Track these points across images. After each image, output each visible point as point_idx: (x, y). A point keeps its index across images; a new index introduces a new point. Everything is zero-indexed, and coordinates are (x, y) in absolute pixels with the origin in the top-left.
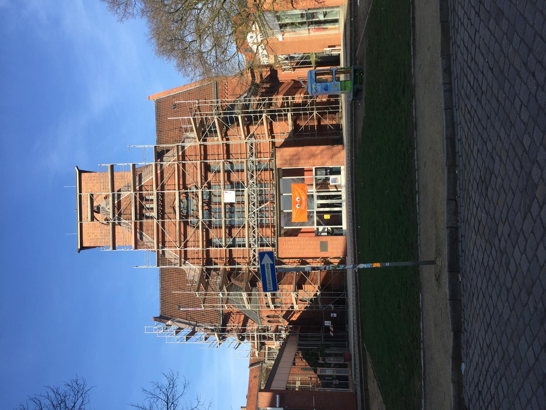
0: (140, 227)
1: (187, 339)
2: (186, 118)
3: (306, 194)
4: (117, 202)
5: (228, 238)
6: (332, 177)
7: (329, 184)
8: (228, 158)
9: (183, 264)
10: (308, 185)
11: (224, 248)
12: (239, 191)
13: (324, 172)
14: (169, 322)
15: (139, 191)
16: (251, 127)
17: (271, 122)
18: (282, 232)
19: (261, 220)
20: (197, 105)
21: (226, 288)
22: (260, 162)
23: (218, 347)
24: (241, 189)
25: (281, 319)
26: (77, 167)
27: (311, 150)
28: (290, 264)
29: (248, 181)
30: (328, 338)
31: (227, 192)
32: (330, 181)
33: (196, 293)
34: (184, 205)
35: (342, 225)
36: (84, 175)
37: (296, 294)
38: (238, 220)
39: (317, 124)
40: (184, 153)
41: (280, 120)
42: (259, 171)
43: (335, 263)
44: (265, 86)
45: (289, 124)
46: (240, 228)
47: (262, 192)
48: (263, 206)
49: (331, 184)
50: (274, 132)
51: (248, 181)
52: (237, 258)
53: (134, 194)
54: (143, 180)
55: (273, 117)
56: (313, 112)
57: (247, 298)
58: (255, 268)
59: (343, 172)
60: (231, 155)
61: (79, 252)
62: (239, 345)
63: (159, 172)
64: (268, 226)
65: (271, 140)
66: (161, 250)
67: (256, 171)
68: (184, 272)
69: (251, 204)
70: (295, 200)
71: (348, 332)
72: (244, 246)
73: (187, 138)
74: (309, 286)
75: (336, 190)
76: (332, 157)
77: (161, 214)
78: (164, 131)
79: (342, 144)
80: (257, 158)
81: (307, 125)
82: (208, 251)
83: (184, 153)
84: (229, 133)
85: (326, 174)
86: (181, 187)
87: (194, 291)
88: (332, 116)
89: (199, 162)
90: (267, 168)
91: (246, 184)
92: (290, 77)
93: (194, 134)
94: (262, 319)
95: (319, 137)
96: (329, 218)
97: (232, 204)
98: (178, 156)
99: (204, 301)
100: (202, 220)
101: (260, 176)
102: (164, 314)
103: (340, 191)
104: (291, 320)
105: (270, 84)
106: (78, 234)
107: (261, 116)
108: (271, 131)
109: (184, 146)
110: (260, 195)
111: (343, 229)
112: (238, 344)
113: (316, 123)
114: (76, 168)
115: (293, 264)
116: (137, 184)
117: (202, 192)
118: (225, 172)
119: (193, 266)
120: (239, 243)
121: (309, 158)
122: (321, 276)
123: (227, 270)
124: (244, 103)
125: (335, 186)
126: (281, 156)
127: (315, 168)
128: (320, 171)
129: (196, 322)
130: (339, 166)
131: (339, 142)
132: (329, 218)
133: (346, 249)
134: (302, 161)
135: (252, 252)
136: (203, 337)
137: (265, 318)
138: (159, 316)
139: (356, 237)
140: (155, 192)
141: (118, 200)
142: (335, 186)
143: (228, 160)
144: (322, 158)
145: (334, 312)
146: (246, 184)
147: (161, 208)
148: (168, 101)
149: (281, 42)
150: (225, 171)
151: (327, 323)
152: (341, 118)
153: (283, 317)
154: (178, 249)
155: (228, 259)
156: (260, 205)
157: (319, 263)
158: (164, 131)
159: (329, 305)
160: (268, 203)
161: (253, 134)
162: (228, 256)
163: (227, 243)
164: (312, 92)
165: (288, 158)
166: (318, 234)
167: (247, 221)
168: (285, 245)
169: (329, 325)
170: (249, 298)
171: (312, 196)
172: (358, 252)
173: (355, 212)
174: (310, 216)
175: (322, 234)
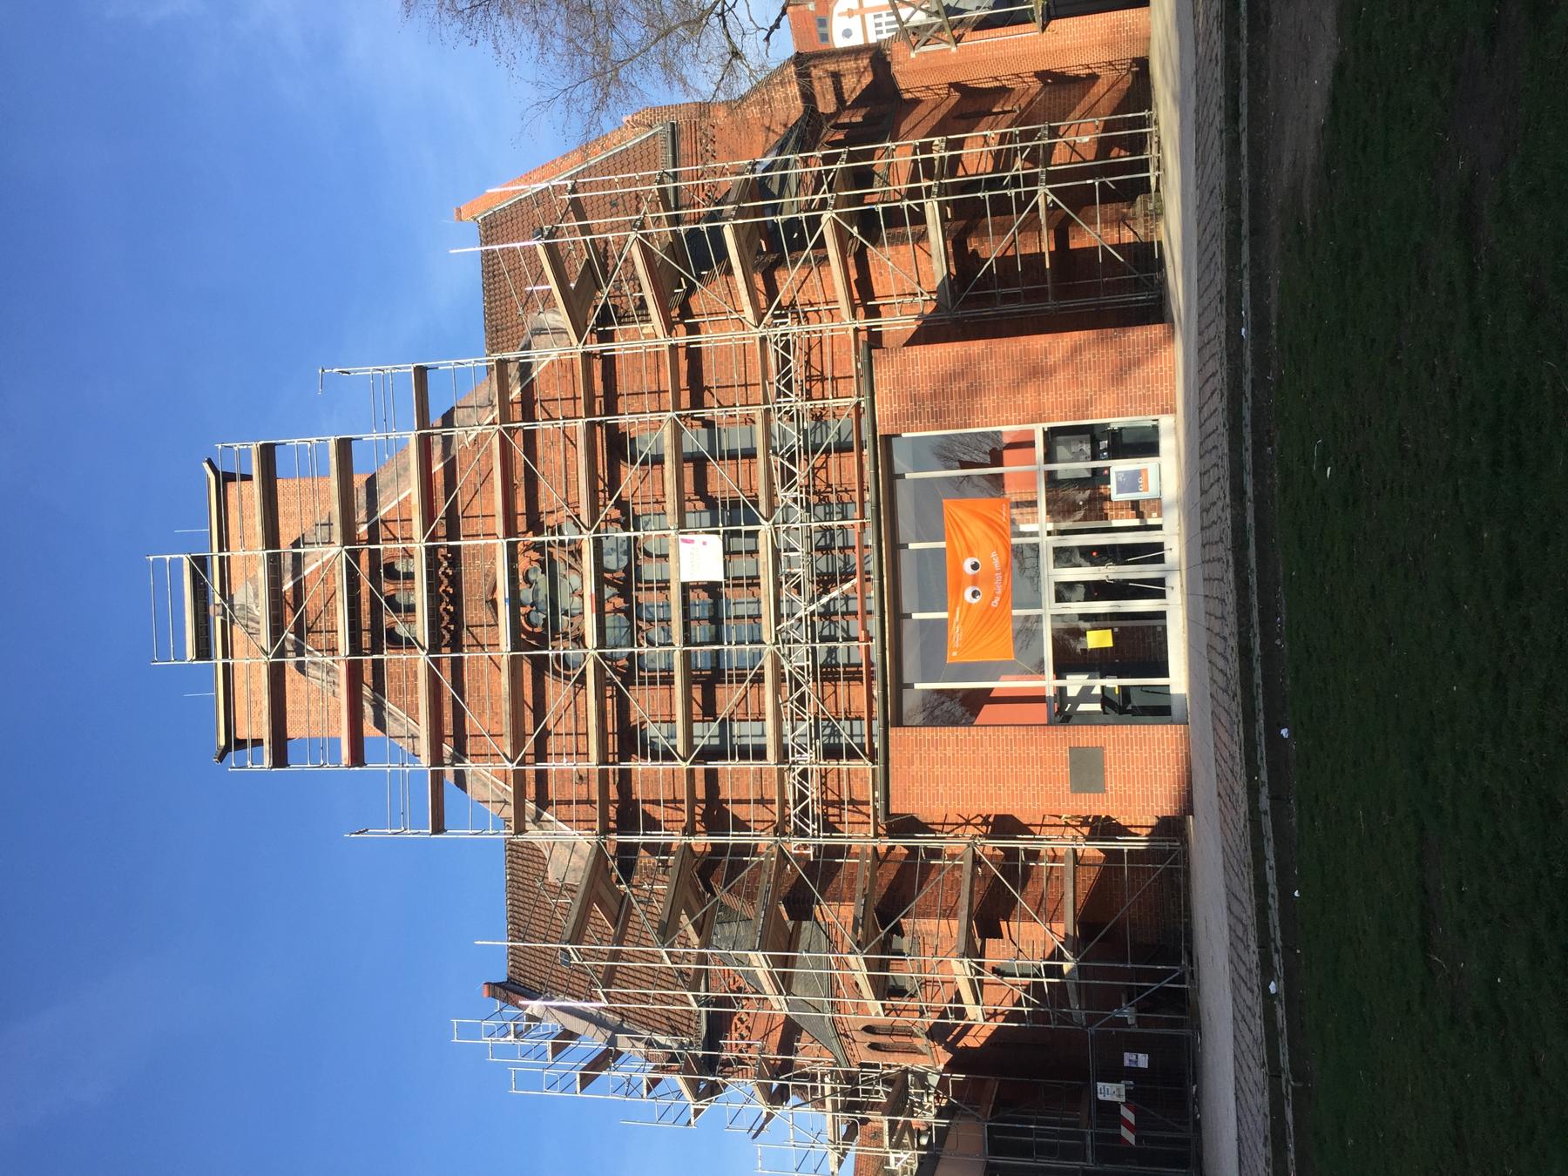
0: (374, 678)
1: (586, 1081)
2: (518, 245)
4: (291, 583)
5: (703, 721)
6: (1119, 467)
7: (1108, 498)
8: (697, 402)
10: (1018, 505)
11: (685, 765)
12: (737, 534)
13: (1087, 448)
14: (535, 1006)
15: (370, 542)
17: (863, 248)
18: (910, 701)
19: (832, 652)
20: (567, 197)
21: (695, 925)
22: (821, 415)
23: (689, 1122)
24: (744, 528)
25: (921, 1042)
26: (210, 462)
27: (1026, 352)
28: (947, 828)
29: (771, 496)
30: (1111, 1149)
32: (1113, 486)
33: (569, 947)
35: (1166, 675)
36: (233, 488)
37: (971, 967)
39: (1053, 248)
40: (528, 392)
41: (897, 240)
43: (1138, 831)
45: (934, 252)
47: (833, 539)
48: (835, 593)
49: (1115, 497)
51: (771, 496)
53: (344, 553)
54: (381, 499)
56: (1036, 191)
58: (805, 847)
59: (1171, 443)
60: (706, 394)
61: (221, 758)
62: (767, 1120)
63: (437, 467)
64: (853, 676)
65: (862, 323)
67: (806, 452)
69: (784, 586)
71: (1198, 1125)
72: (760, 753)
73: (540, 331)
74: (1025, 926)
75: (1136, 522)
76: (1120, 375)
77: (449, 631)
78: (508, 328)
79: (1161, 320)
80: (809, 398)
81: (1010, 253)
82: (625, 776)
83: (528, 392)
85: (1095, 457)
86: (521, 523)
88: (1117, 211)
89: (581, 424)
91: (763, 508)
92: (942, 69)
93: (559, 317)
94: (847, 1036)
95: (1064, 303)
96: (1109, 643)
97: (712, 588)
98: (505, 405)
99: (609, 978)
100: (595, 653)
102: (520, 975)
103: (1159, 527)
104: (960, 1045)
105: (863, 111)
106: (217, 695)
108: (863, 292)
109: (530, 364)
110: (826, 549)
111: (1173, 691)
112: (764, 1115)
113: (1047, 245)
114: (206, 466)
115: (959, 831)
116: (361, 515)
118: (686, 461)
121: (1017, 386)
122: (1080, 886)
124: (751, 176)
125: (1133, 509)
126: (898, 381)
127: (1045, 433)
128: (1067, 444)
129: (622, 1014)
130: (1145, 421)
131: (1155, 311)
132: (1109, 643)
133: (1189, 778)
134: (988, 401)
135: (792, 780)
136: (644, 1078)
137: (858, 1036)
138: (504, 979)
139: (1265, 791)
142: (1135, 505)
143: (698, 413)
144: (1076, 382)
146: (763, 508)
148: (520, 219)
150: (682, 458)
151: (1110, 1092)
152: (1158, 213)
153: (926, 1034)
154: (511, 767)
155: (704, 806)
156: (827, 592)
158: (508, 328)
159: (1116, 1013)
160: (856, 581)
161: (793, 305)
162: (701, 793)
163: (696, 741)
165: (925, 387)
166: (1063, 712)
168: (917, 762)
169: (1115, 1099)
171: (1035, 548)
172: (1285, 895)
173: (1256, 643)
175: (1083, 707)
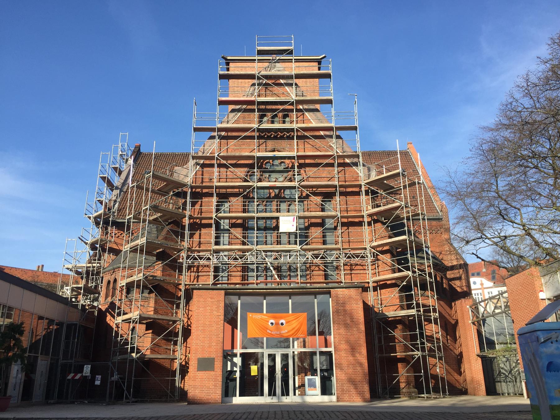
0: (249, 109)
1: (103, 178)
3: (291, 336)
4: (283, 82)
5: (229, 223)
6: (317, 380)
7: (306, 375)
8: (343, 224)
9: (196, 163)
11: (214, 216)
12: (296, 237)
13: (325, 367)
16: (389, 255)
17: (398, 286)
18: (234, 298)
19: (253, 270)
20: (416, 181)
21: (157, 218)
23: (86, 215)
24: (298, 240)
26: (325, 57)
27: (360, 346)
29: (310, 250)
31: (294, 221)
32: (310, 377)
33: (151, 173)
34: (277, 165)
35: (240, 395)
37: (136, 319)
38: (254, 241)
39: (398, 357)
40: (348, 165)
41: (401, 299)
42: (325, 266)
43: (183, 383)
44: (444, 282)
45: (397, 312)
46: (243, 238)
48: (274, 272)
49: (307, 378)
50: (383, 291)
51: (310, 250)
52: (200, 234)
54: (311, 113)
55: (407, 288)
57: (138, 245)
58: (183, 259)
60: (346, 228)
61: (223, 57)
63: (322, 133)
64: (244, 278)
65: (371, 285)
66: (216, 134)
68: (185, 163)
69: (277, 254)
70: (282, 318)
71: (73, 403)
73: (369, 170)
75: (297, 386)
76: (352, 381)
77: (265, 135)
78: (370, 159)
80: (344, 265)
81: (396, 341)
83: (348, 165)
84: (379, 225)
85: (321, 370)
86: (302, 161)
87: (153, 171)
88: (412, 382)
89: (336, 183)
90: (329, 279)
91: (305, 247)
93: (374, 177)
94: (113, 272)
95: (378, 361)
97: (277, 228)
98: (343, 157)
100: (255, 186)
101: (318, 269)
102: (142, 157)
103: (295, 394)
104: (108, 314)
105: (447, 288)
107: (408, 269)
108: (382, 286)
109: (357, 166)
110: (290, 269)
111: (234, 398)
112: (87, 242)
113: (399, 355)
114: (324, 56)
115: (186, 316)
116: (306, 107)
117: (294, 188)
118: (323, 220)
119: (192, 175)
120: (222, 238)
123: (299, 393)
126: (350, 297)
128: (326, 360)
129: (126, 192)
130: (334, 390)
131: (375, 395)
134: (342, 331)
135: (207, 254)
136: (103, 199)
137: (113, 276)
138: (141, 151)
140: (295, 126)
141: (285, 83)
142: (303, 385)
143: (340, 224)
145: (103, 381)
146: (305, 247)
147: (272, 136)
148: (408, 164)
149: (537, 297)
150: (323, 218)
151: (87, 369)
153: (112, 302)
154: (216, 155)
155: (199, 222)
157: (184, 357)
158: (370, 159)
160: (278, 280)
161: (378, 260)
162: (204, 222)
163: (222, 220)
164: (539, 333)
165: (348, 308)
166: (228, 356)
167: (251, 248)
169: (84, 371)
170: (137, 250)
171: (288, 347)
174: (257, 343)
175: (229, 363)
